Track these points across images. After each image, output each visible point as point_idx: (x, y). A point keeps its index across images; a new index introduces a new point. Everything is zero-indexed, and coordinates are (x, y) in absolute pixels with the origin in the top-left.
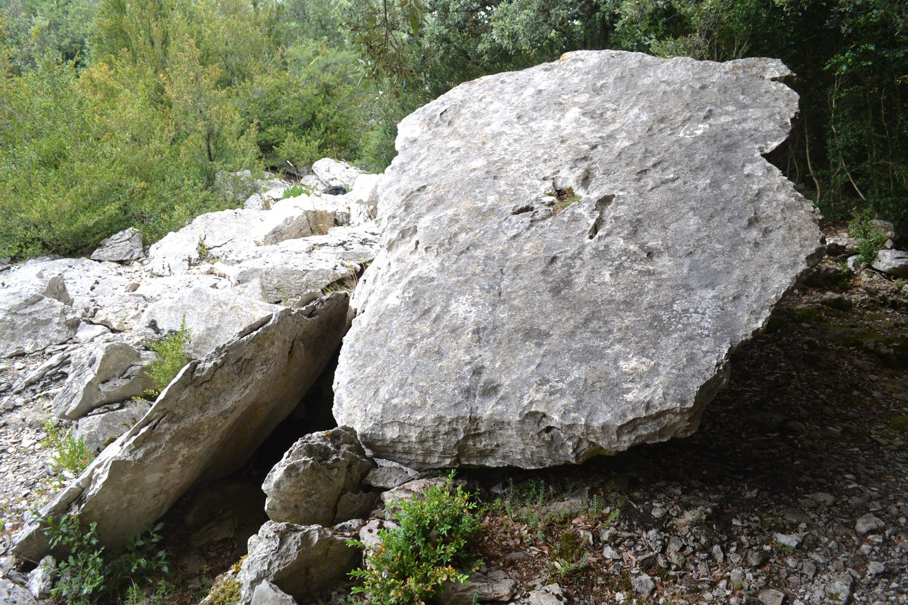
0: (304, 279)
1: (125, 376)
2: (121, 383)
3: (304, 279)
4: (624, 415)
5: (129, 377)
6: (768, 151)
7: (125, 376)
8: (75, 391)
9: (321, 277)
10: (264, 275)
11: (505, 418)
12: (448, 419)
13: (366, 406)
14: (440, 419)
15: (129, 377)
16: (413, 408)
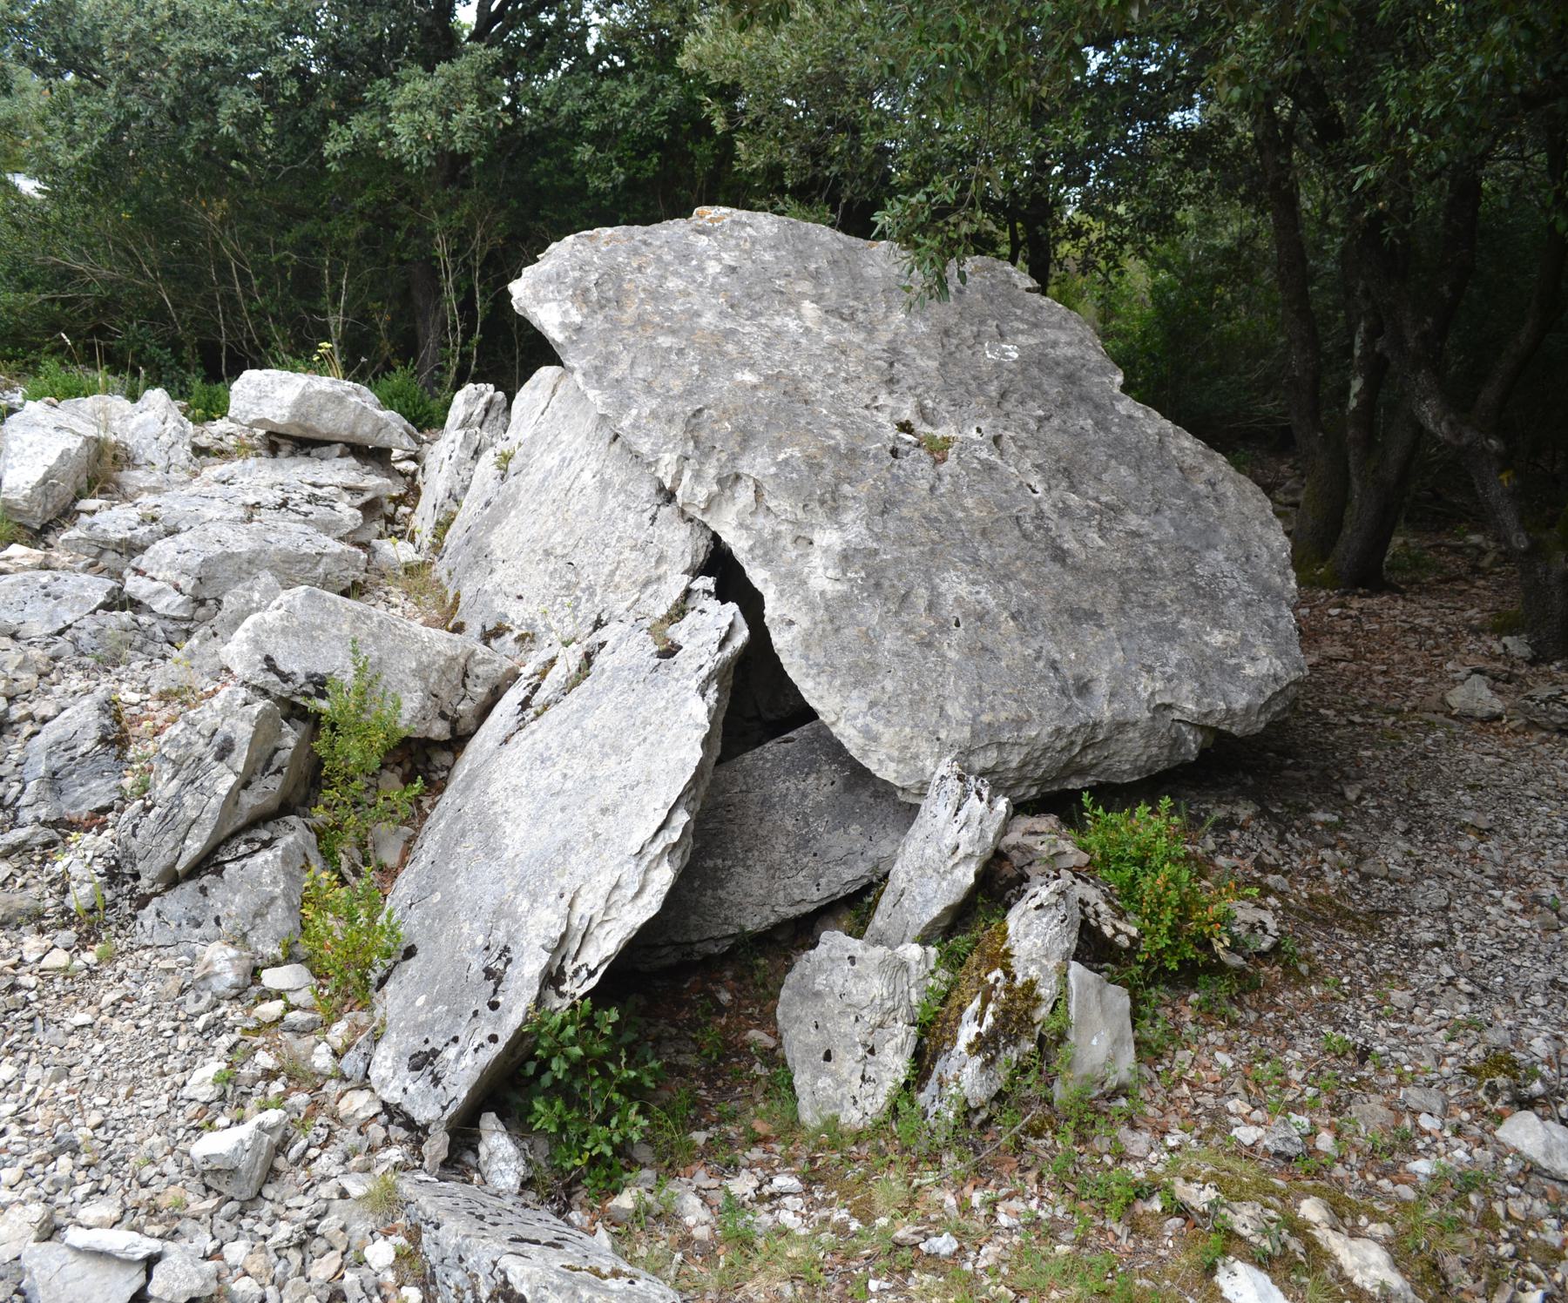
0: (321, 570)
1: (273, 769)
2: (274, 783)
3: (321, 570)
4: (1261, 692)
5: (279, 771)
6: (546, 373)
7: (273, 769)
8: (194, 814)
9: (345, 565)
10: (245, 566)
11: (1130, 717)
12: (1069, 729)
13: (935, 733)
14: (1058, 731)
15: (279, 771)
16: (1019, 723)
